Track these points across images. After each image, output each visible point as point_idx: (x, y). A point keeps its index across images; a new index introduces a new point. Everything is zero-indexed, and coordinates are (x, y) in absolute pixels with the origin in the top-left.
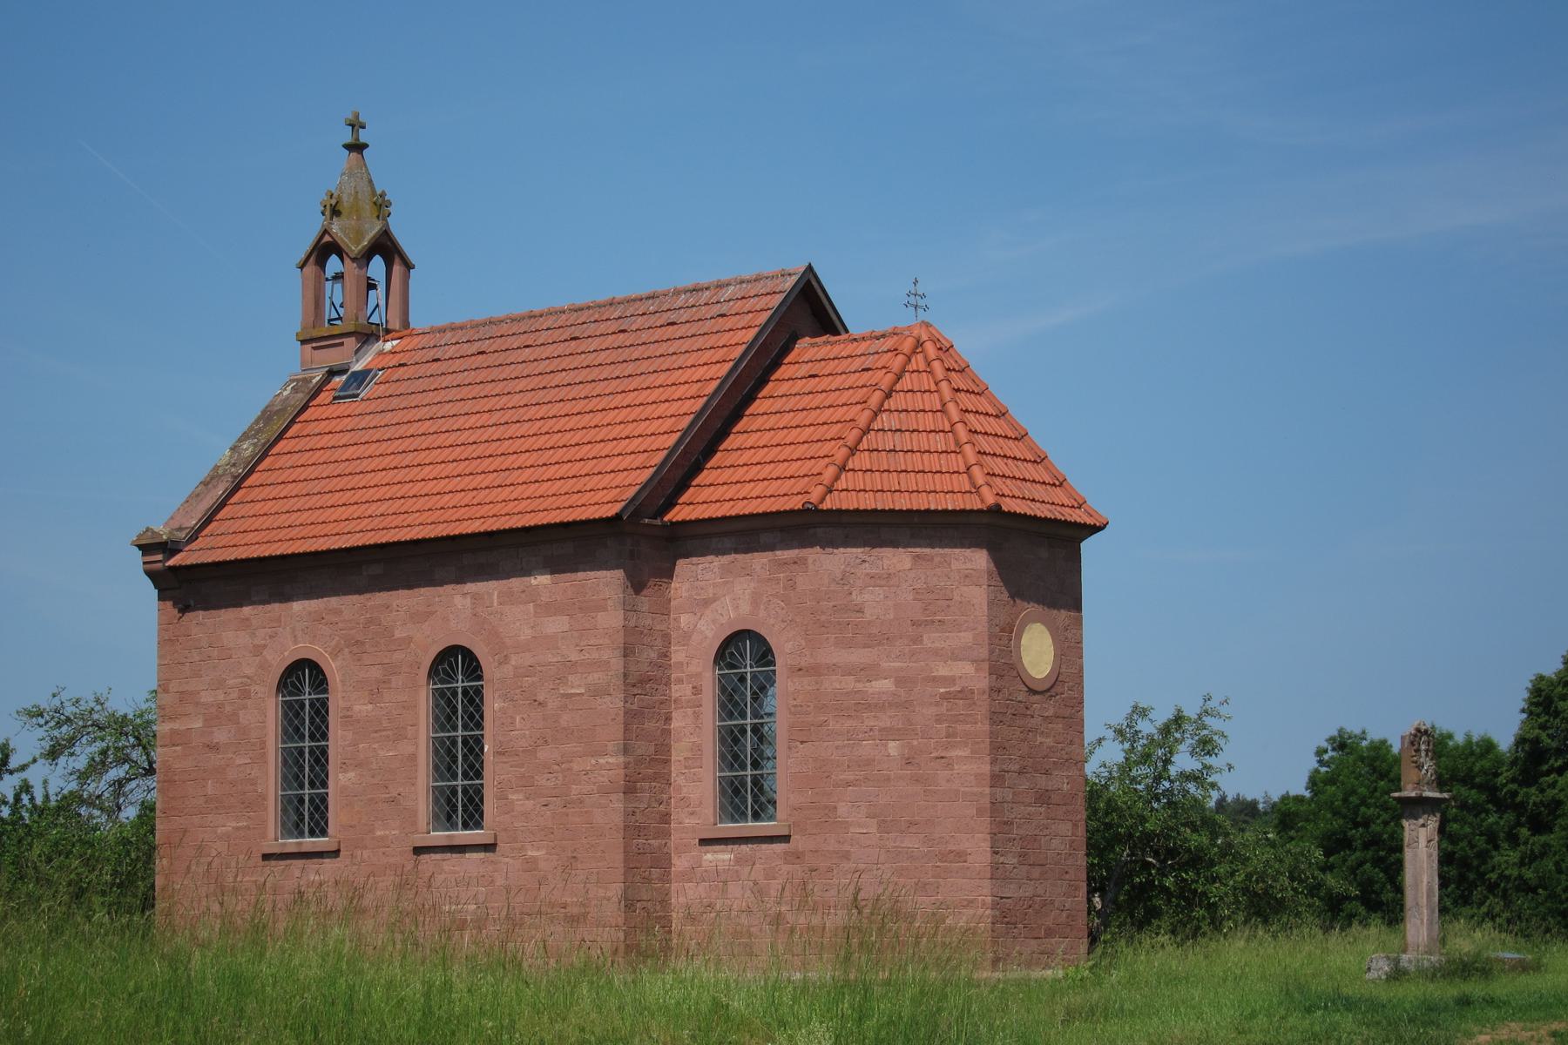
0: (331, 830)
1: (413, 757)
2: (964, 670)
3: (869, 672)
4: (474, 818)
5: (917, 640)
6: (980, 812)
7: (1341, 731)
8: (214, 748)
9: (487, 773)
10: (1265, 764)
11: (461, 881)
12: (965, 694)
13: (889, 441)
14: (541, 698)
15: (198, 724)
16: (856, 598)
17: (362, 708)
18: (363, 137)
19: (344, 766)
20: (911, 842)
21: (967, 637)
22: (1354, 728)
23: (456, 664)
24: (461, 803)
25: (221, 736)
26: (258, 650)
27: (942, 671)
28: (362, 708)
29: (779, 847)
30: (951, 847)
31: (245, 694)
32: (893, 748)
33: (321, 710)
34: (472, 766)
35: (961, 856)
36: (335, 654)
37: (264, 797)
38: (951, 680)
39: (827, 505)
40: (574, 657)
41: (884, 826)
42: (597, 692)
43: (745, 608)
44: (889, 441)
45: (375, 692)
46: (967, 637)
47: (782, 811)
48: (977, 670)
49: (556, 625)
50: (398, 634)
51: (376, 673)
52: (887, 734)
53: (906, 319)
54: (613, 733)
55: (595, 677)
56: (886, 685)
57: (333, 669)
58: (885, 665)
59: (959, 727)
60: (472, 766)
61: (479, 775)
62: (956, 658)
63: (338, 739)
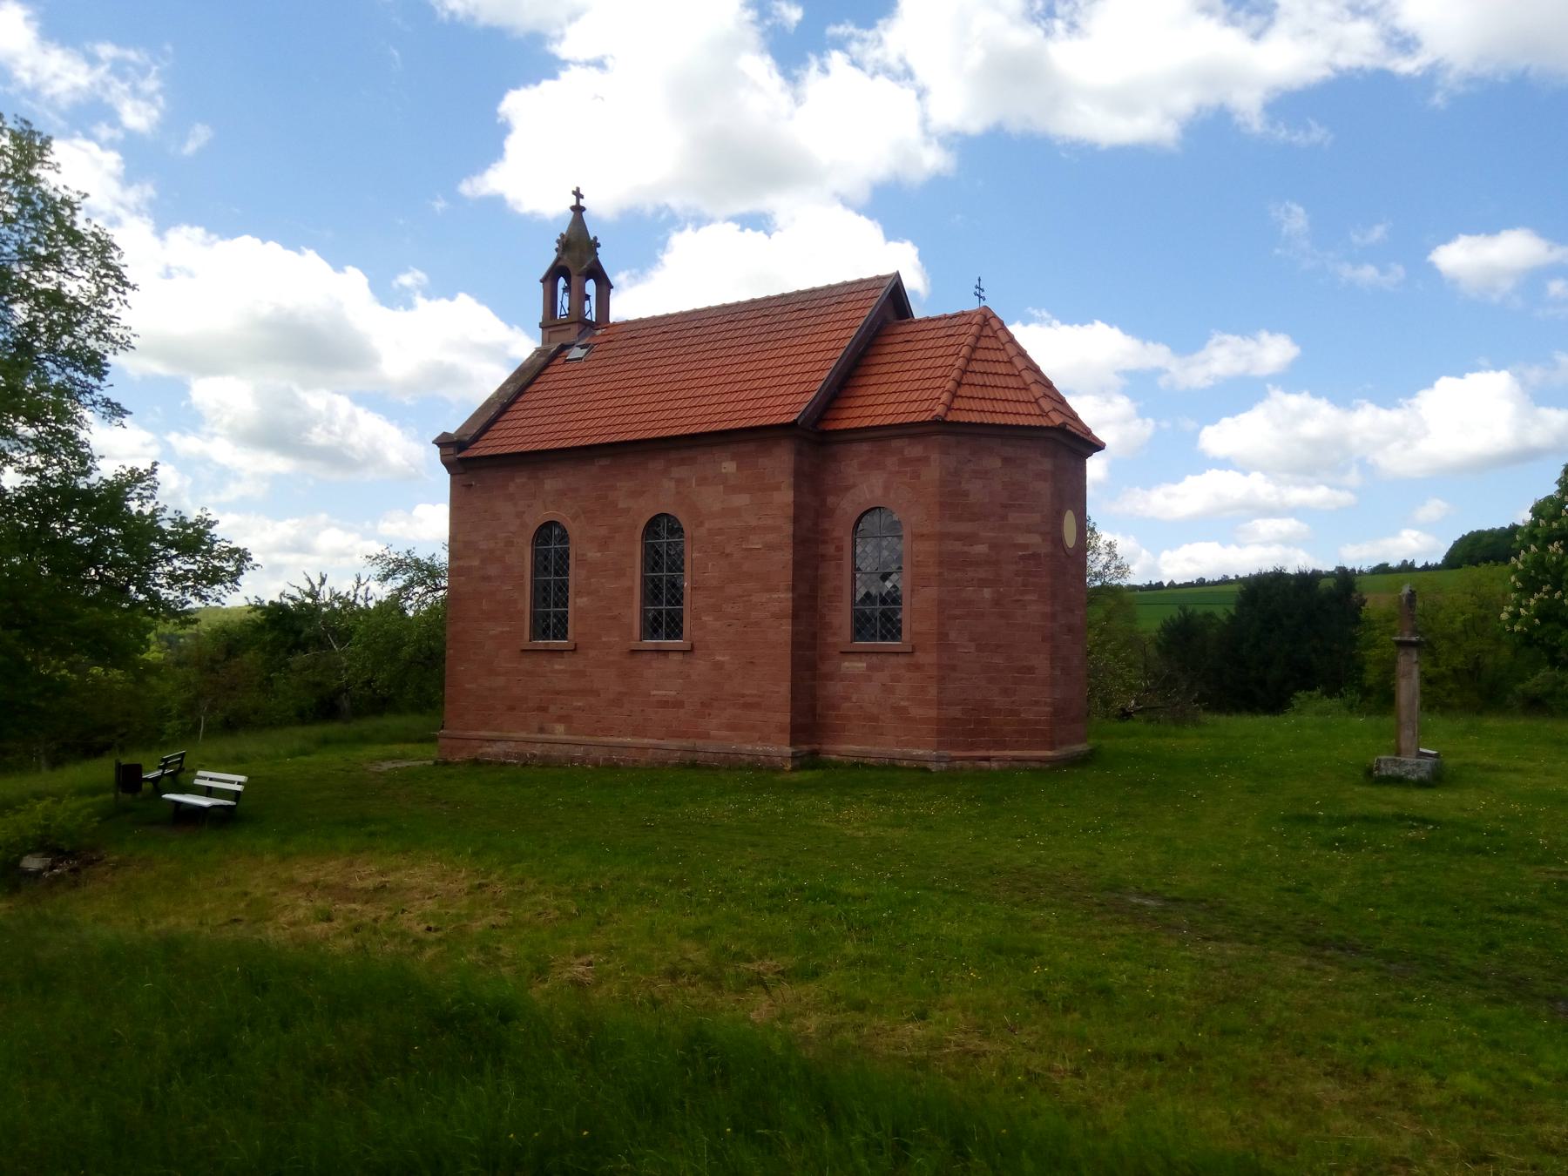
0: (570, 635)
1: (631, 589)
2: (1035, 539)
3: (970, 539)
4: (675, 630)
8: (486, 578)
9: (571, 572)
11: (664, 677)
12: (1035, 556)
13: (978, 379)
14: (728, 551)
15: (476, 563)
16: (965, 486)
17: (593, 555)
18: (582, 203)
19: (578, 594)
21: (1036, 518)
23: (661, 528)
24: (663, 618)
25: (493, 570)
26: (519, 515)
27: (1021, 539)
28: (593, 555)
29: (903, 660)
31: (509, 543)
32: (987, 593)
33: (564, 556)
34: (673, 596)
35: (1031, 669)
36: (575, 518)
37: (522, 612)
38: (1025, 547)
39: (949, 418)
40: (754, 523)
42: (770, 547)
43: (879, 492)
44: (978, 379)
45: (604, 544)
47: (905, 635)
49: (742, 500)
50: (621, 505)
51: (603, 531)
52: (983, 583)
53: (972, 305)
54: (786, 577)
55: (771, 537)
56: (981, 549)
57: (573, 529)
60: (673, 596)
61: (679, 602)
62: (1029, 531)
63: (575, 576)
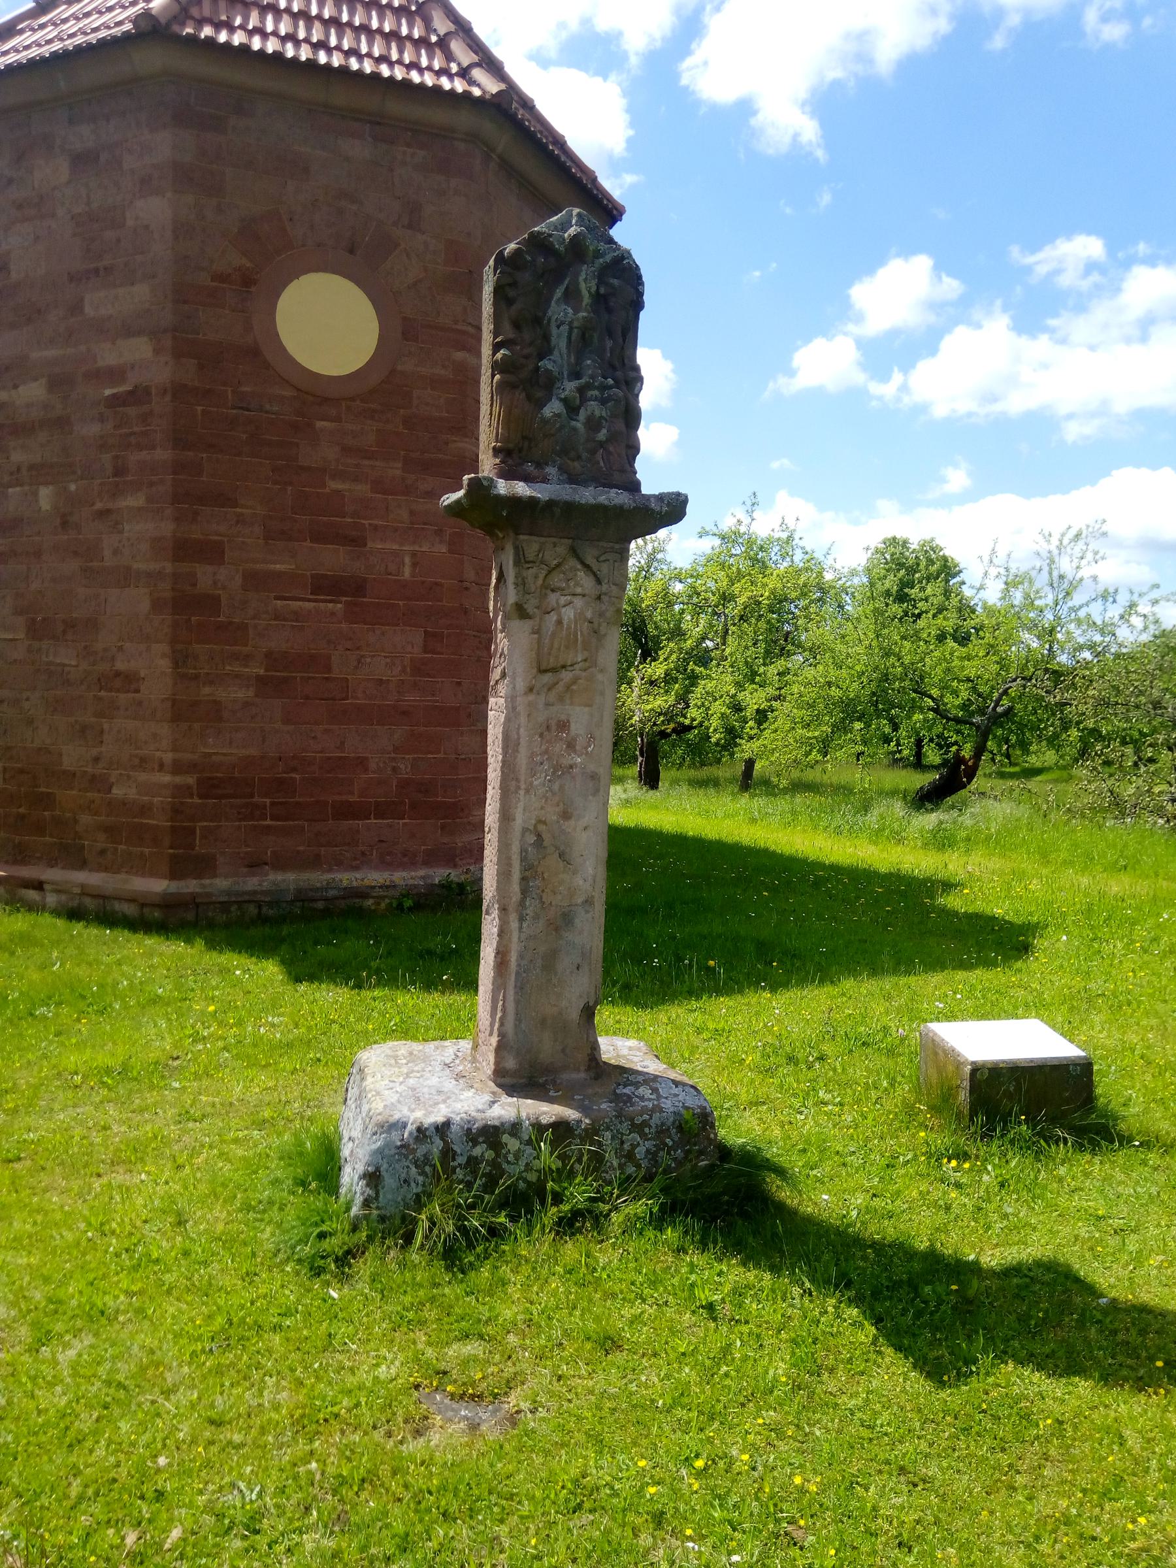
5: (76, 308)
6: (157, 605)
7: (586, 22)
10: (1003, 586)
12: (138, 395)
20: (65, 656)
21: (141, 292)
22: (939, 542)
27: (109, 355)
30: (120, 665)
32: (46, 497)
35: (130, 681)
38: (115, 374)
41: (36, 631)
46: (141, 292)
48: (157, 351)
52: (40, 473)
56: (32, 392)
58: (35, 355)
59: (134, 458)
